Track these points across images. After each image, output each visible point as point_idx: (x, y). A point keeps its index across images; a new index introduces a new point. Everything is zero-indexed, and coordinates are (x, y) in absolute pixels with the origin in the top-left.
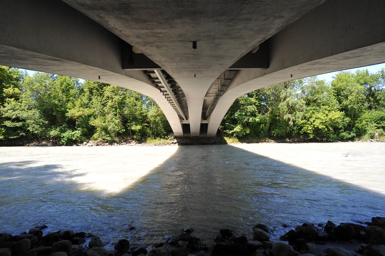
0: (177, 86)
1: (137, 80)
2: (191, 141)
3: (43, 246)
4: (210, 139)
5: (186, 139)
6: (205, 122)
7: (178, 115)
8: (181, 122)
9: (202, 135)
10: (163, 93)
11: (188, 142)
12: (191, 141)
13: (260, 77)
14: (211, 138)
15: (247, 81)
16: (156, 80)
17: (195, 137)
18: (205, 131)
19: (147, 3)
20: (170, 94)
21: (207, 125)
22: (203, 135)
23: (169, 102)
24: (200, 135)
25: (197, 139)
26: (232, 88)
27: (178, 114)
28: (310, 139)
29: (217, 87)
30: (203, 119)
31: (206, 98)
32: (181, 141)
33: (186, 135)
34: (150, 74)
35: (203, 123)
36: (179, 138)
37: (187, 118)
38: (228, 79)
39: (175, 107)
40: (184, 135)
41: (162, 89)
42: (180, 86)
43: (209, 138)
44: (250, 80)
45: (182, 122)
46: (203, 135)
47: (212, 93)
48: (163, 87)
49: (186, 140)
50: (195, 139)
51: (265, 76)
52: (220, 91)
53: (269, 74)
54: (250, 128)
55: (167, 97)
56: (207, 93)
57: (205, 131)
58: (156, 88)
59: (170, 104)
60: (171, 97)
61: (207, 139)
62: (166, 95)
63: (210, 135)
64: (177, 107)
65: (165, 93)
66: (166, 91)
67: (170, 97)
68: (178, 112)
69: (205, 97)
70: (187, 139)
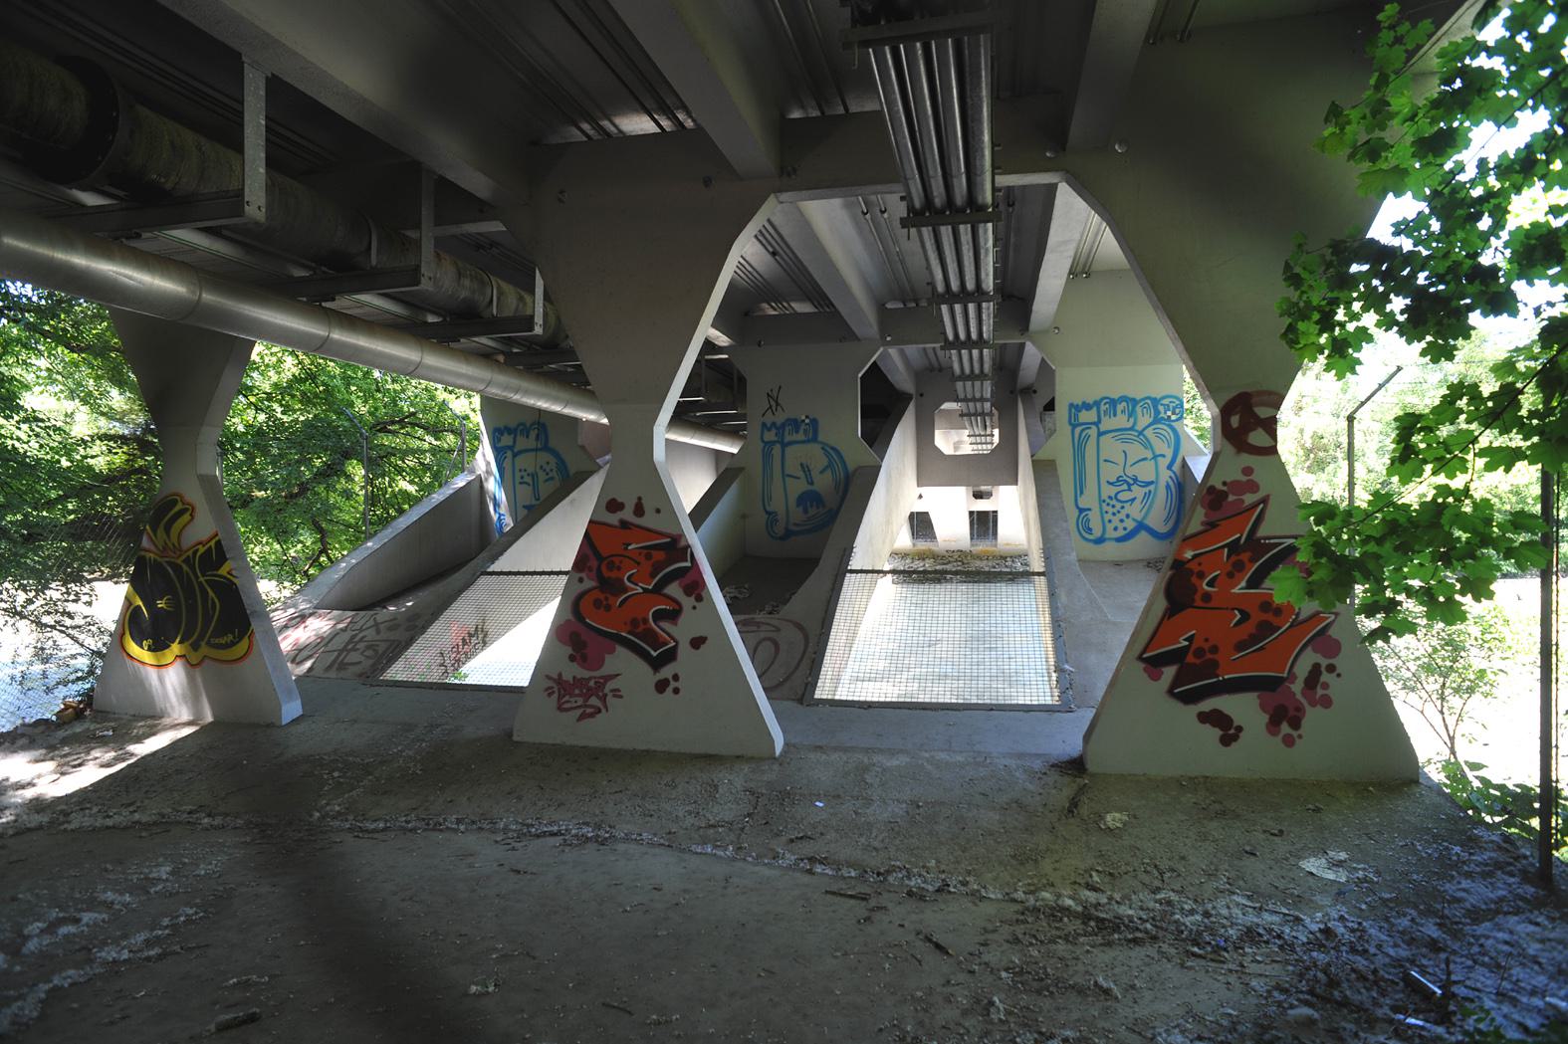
3: (1195, 664)
4: (1008, 559)
19: (944, 1027)
22: (983, 546)
24: (972, 545)
28: (1554, 396)
33: (923, 545)
40: (914, 545)
43: (1004, 558)
46: (983, 546)
49: (921, 564)
50: (956, 561)
57: (1270, 592)
63: (1008, 547)
70: (927, 561)
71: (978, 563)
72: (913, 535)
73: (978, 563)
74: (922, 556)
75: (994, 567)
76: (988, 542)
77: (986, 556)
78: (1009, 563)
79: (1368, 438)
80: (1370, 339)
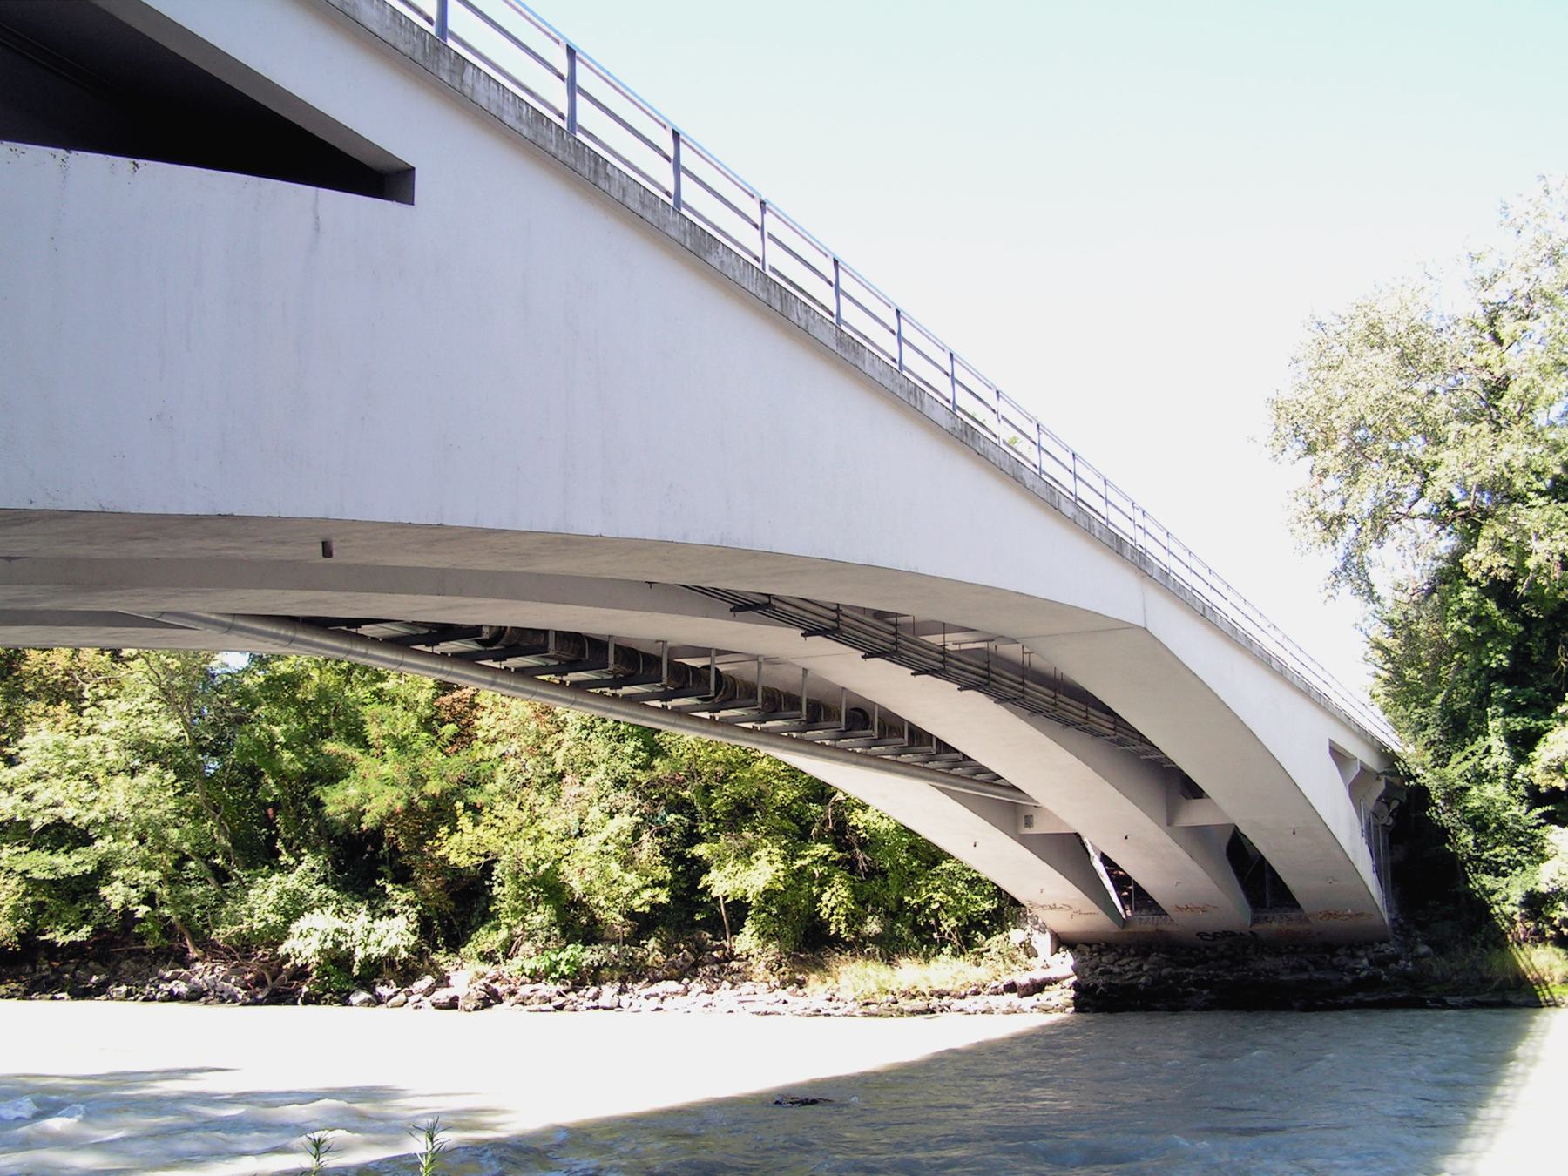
9: (1275, 925)
17: (1215, 935)
73: (1269, 962)
77: (1274, 947)
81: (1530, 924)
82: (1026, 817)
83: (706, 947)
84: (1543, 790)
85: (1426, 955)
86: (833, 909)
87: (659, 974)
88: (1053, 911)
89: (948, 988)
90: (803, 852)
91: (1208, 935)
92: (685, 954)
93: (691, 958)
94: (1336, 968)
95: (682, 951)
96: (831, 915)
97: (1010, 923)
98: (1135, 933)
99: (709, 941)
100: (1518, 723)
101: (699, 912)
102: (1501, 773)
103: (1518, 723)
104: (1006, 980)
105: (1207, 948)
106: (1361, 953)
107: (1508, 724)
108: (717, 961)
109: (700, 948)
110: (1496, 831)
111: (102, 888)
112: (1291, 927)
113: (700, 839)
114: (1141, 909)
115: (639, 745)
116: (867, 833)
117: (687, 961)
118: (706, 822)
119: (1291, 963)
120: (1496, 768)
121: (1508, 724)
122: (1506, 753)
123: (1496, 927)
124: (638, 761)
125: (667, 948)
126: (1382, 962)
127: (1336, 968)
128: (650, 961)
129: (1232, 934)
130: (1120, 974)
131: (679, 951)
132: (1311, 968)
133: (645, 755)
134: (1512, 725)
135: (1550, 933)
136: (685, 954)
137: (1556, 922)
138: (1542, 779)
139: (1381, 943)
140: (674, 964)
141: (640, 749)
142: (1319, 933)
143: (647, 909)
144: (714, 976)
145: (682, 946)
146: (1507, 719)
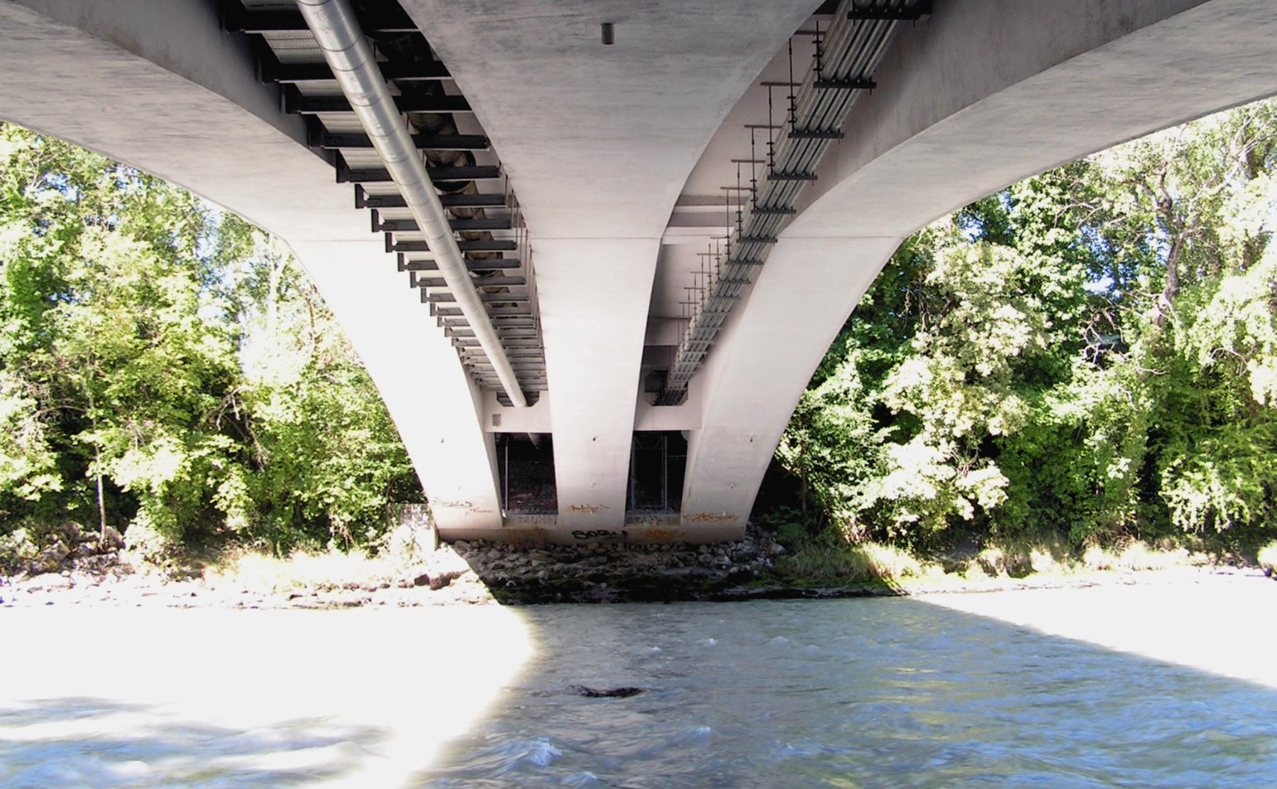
0: (462, 130)
1: (163, 74)
2: (557, 566)
5: (525, 551)
6: (664, 420)
7: (467, 368)
8: (491, 421)
9: (646, 525)
10: (359, 191)
11: (541, 574)
12: (557, 566)
13: (1087, 50)
14: (709, 545)
15: (988, 91)
16: (308, 86)
17: (589, 534)
18: (665, 493)
20: (407, 195)
21: (677, 443)
22: (649, 523)
23: (413, 277)
25: (602, 555)
26: (876, 156)
27: (462, 359)
29: (762, 151)
30: (653, 397)
31: (677, 237)
32: (485, 563)
33: (526, 521)
34: (263, 32)
35: (649, 425)
36: (467, 546)
37: (533, 388)
38: (849, 82)
39: (441, 298)
41: (353, 156)
42: (462, 98)
44: (1008, 79)
45: (496, 420)
46: (649, 523)
47: (724, 193)
48: (361, 140)
49: (523, 560)
50: (594, 554)
51: (1124, 39)
52: (785, 175)
53: (1155, 29)
54: (1005, 469)
55: (422, 280)
56: (682, 200)
57: (665, 493)
58: (305, 149)
59: (407, 273)
60: (456, 296)
61: (681, 554)
62: (378, 201)
63: (703, 524)
64: (461, 303)
65: (371, 188)
66: (398, 201)
67: (459, 309)
68: (461, 341)
69: (673, 230)
71: (642, 559)
72: (503, 502)
73: (642, 559)
74: (523, 543)
75: (674, 565)
76: (662, 515)
77: (657, 544)
78: (705, 556)
79: (1260, 325)
80: (677, 443)
81: (863, 527)
82: (494, 416)
83: (78, 538)
84: (893, 413)
85: (781, 553)
86: (231, 501)
87: (39, 566)
88: (452, 508)
89: (357, 582)
90: (201, 443)
91: (582, 533)
92: (58, 546)
93: (66, 549)
94: (701, 565)
95: (56, 542)
96: (229, 507)
97: (394, 519)
98: (515, 531)
99: (82, 533)
100: (873, 355)
101: (71, 502)
102: (850, 396)
103: (873, 355)
104: (417, 572)
105: (579, 546)
106: (721, 551)
107: (865, 355)
108: (92, 553)
109: (73, 540)
110: (845, 446)
111: (38, 500)
112: (662, 527)
113: (87, 425)
114: (513, 508)
115: (26, 323)
116: (270, 425)
117: (63, 552)
118: (93, 408)
119: (665, 560)
120: (846, 393)
121: (865, 355)
122: (857, 379)
123: (838, 534)
124: (25, 340)
125: (40, 539)
126: (742, 559)
127: (701, 565)
128: (21, 552)
129: (606, 533)
130: (513, 569)
131: (52, 542)
132: (682, 565)
133: (32, 335)
134: (869, 355)
135: (892, 534)
136: (58, 546)
137: (898, 525)
138: (894, 404)
139: (737, 542)
140: (51, 556)
141: (26, 328)
142: (683, 533)
143: (37, 497)
144: (92, 568)
145: (55, 537)
146: (865, 351)
